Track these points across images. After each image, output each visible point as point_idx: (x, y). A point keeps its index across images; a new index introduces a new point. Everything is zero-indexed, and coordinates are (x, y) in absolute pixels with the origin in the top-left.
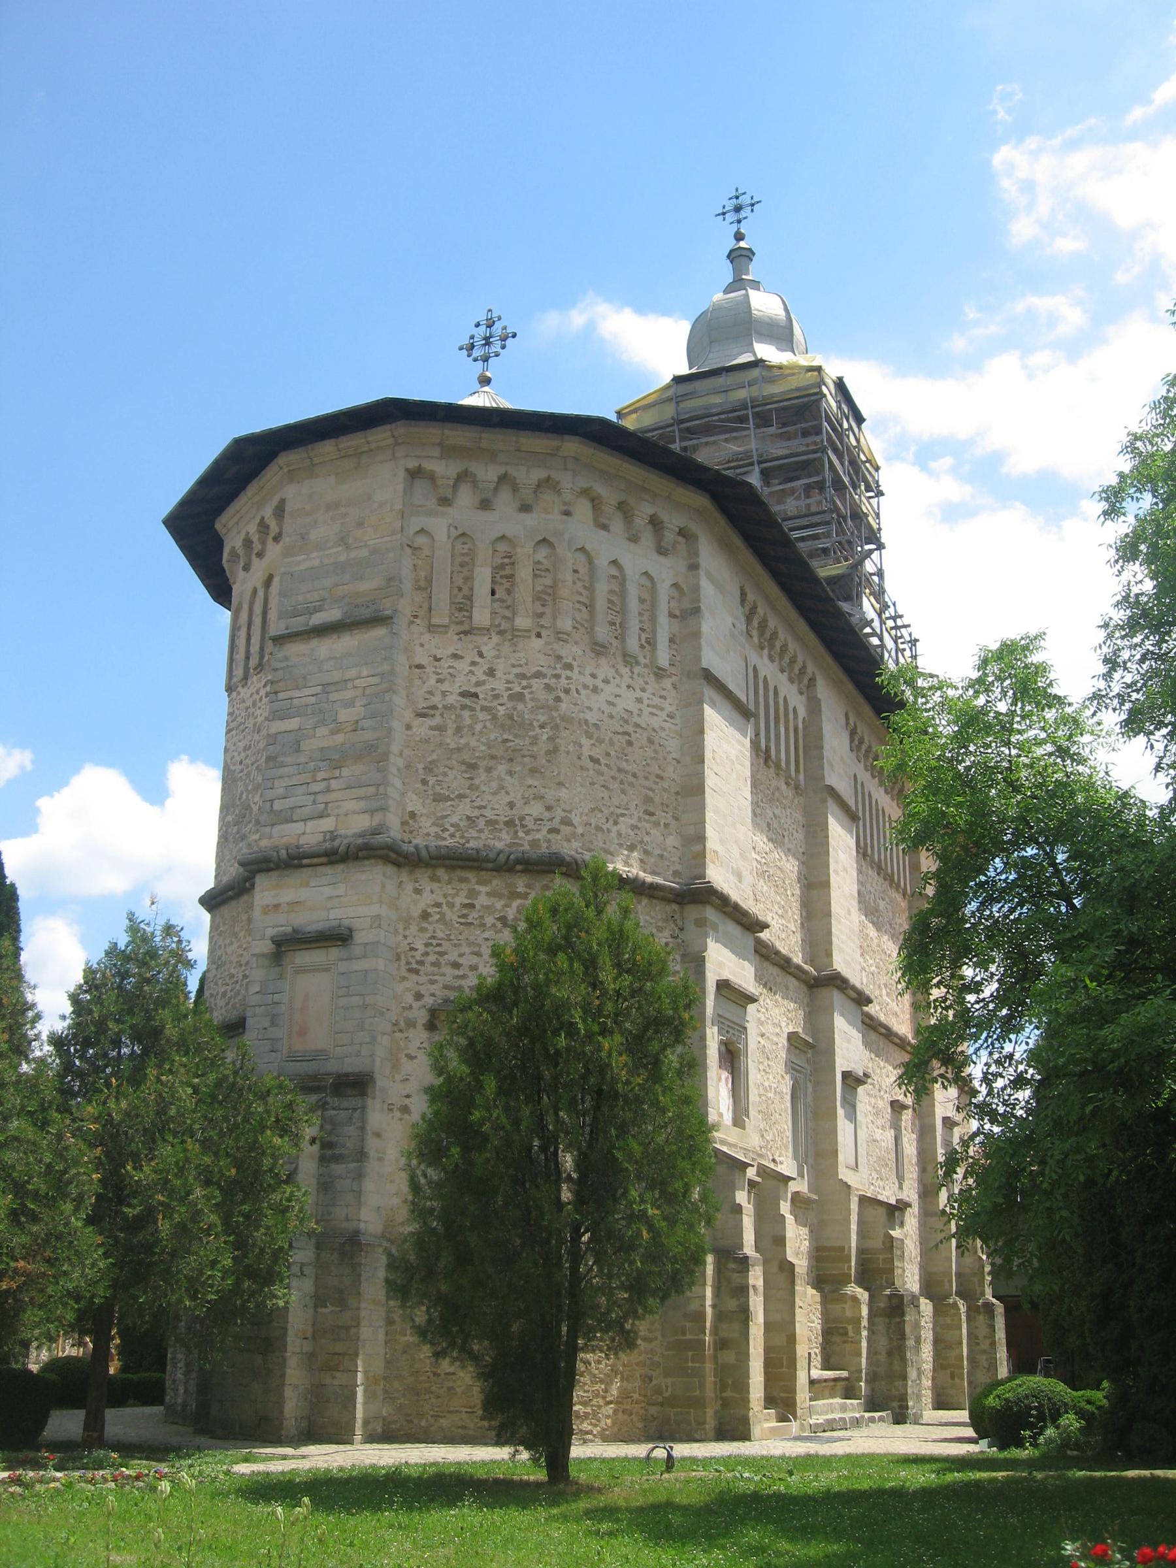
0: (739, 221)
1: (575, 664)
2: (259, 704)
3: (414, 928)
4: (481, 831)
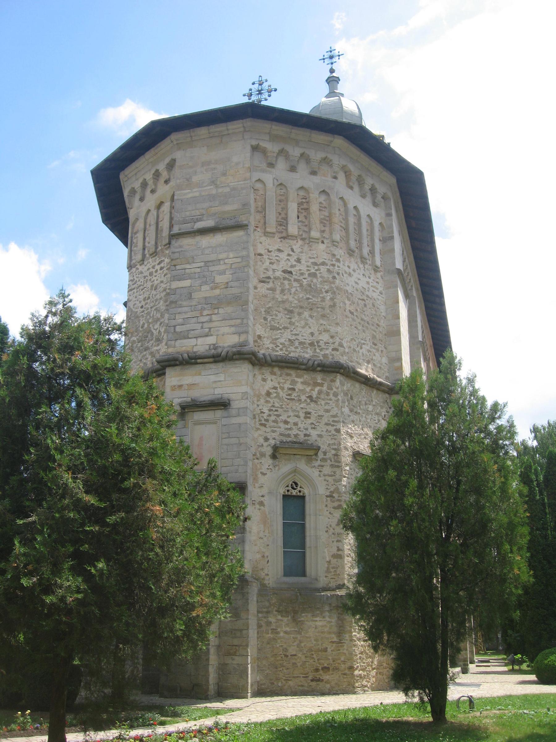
0: (332, 64)
1: (341, 259)
2: (154, 274)
3: (262, 401)
4: (296, 348)
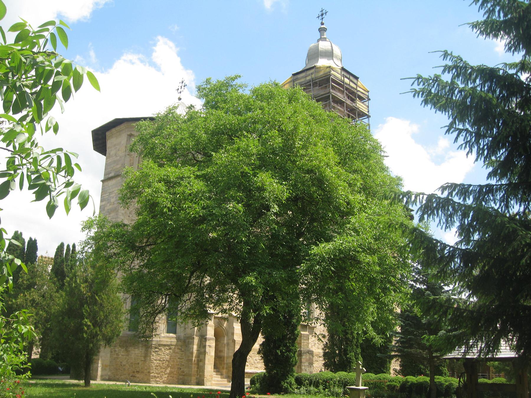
0: (322, 19)
